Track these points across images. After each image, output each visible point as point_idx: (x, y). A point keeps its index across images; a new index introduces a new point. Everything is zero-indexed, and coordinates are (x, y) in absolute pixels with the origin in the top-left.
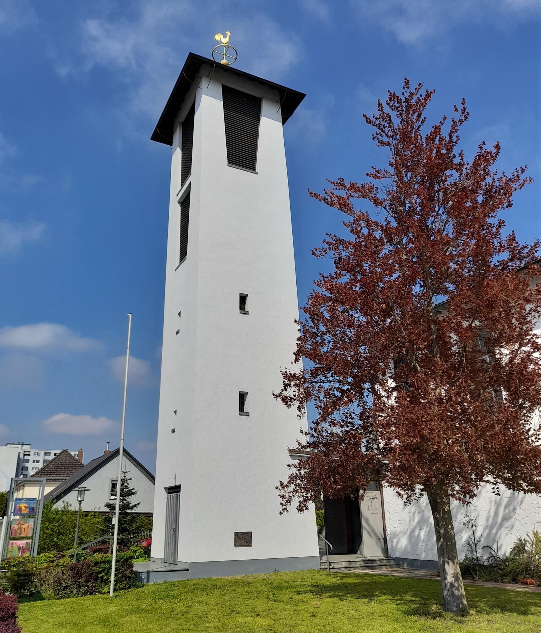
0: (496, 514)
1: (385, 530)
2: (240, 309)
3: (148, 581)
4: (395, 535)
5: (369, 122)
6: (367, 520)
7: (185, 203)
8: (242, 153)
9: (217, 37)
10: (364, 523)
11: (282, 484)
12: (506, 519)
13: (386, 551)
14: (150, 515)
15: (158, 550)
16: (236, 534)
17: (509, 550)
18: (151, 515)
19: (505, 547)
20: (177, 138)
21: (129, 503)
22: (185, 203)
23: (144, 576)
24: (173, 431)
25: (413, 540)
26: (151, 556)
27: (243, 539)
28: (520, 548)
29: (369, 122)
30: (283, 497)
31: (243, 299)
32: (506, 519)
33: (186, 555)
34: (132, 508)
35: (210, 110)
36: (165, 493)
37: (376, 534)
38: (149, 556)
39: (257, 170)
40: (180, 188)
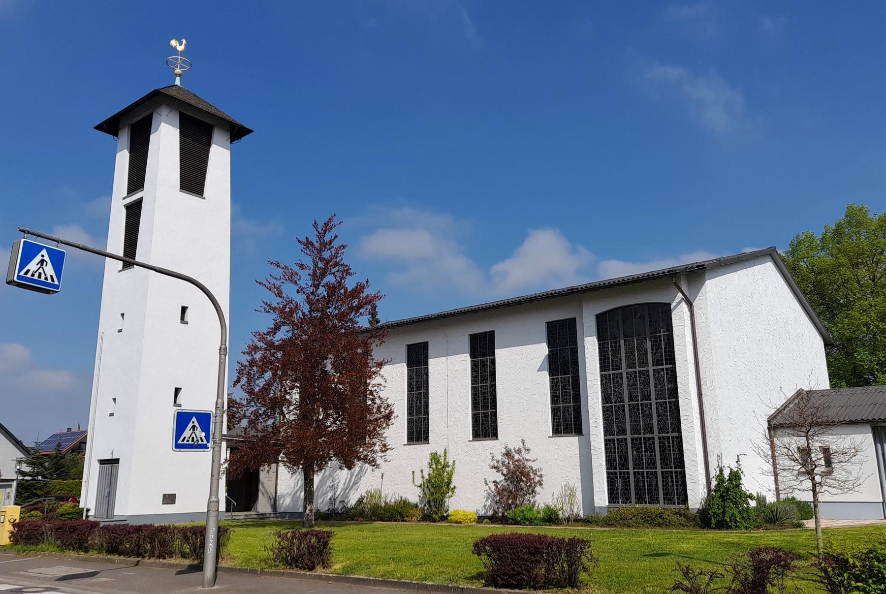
0: (350, 480)
1: (276, 492)
4: (283, 496)
5: (299, 242)
6: (263, 484)
7: (134, 211)
8: (193, 180)
9: (174, 43)
10: (260, 487)
12: (355, 483)
13: (274, 507)
16: (164, 495)
17: (354, 503)
19: (352, 501)
22: (134, 211)
25: (294, 498)
27: (169, 499)
28: (360, 501)
29: (299, 242)
31: (184, 309)
32: (355, 483)
35: (166, 140)
36: (98, 465)
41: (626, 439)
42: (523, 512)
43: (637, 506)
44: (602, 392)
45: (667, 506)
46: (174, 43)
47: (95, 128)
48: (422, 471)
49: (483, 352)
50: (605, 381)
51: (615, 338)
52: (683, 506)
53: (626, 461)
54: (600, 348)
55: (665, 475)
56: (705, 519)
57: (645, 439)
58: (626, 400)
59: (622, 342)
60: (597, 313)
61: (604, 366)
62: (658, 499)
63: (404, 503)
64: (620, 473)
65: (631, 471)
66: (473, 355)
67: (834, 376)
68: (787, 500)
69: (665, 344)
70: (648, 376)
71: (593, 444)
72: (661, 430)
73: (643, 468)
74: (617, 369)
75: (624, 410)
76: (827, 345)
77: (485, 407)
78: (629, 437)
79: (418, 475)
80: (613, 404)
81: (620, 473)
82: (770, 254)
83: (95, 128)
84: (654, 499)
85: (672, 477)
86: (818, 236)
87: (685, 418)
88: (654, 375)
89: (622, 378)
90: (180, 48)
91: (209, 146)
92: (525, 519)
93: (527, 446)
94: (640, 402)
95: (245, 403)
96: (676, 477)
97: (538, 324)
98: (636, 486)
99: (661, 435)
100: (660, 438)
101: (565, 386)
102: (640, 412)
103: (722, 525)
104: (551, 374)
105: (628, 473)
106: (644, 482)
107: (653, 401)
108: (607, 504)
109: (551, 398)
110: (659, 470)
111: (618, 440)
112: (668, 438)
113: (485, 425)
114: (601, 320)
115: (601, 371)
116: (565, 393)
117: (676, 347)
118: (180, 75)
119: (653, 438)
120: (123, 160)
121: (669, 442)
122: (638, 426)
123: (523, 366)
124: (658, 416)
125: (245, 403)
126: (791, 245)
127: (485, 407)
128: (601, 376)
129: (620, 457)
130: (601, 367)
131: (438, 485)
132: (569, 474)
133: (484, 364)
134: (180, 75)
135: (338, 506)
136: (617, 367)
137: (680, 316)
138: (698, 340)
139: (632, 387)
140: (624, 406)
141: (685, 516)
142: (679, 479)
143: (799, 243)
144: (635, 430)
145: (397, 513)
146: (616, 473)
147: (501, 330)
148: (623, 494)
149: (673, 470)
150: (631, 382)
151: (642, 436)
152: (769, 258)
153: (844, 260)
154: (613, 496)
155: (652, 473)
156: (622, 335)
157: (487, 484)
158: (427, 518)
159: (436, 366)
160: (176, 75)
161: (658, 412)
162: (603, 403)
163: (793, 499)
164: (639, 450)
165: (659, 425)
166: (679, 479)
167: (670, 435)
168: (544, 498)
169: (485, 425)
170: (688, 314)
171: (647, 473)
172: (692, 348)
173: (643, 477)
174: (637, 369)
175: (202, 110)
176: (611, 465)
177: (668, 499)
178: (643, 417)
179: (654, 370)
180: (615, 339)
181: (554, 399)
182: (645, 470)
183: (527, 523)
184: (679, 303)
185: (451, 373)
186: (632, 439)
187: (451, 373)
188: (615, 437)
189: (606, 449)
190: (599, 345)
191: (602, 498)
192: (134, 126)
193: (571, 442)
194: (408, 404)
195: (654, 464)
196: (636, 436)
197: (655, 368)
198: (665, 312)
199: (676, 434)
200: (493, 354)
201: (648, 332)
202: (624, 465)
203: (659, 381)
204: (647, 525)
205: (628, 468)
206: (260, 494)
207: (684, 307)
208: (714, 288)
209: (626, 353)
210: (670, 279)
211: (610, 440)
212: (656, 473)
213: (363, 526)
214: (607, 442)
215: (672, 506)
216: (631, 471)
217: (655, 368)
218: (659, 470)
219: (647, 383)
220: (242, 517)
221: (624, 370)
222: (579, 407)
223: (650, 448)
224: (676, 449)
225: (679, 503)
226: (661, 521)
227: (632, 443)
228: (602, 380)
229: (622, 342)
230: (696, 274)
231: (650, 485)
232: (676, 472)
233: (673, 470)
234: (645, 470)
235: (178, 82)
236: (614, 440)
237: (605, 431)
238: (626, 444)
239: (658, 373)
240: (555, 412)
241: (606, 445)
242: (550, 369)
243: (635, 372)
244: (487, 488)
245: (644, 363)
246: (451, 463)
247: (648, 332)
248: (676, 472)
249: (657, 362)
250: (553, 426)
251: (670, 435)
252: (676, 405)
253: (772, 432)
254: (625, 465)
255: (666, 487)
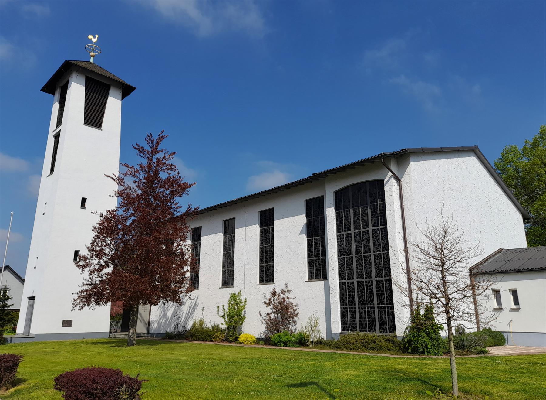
2: (82, 206)
3: (11, 342)
4: (153, 322)
6: (141, 315)
7: (57, 137)
8: (94, 117)
9: (90, 37)
11: (74, 299)
13: (148, 329)
14: (18, 311)
15: (20, 328)
16: (64, 321)
18: (18, 311)
20: (58, 94)
21: (7, 304)
22: (57, 137)
23: (9, 340)
24: (35, 268)
26: (17, 332)
27: (67, 323)
28: (193, 326)
30: (74, 304)
31: (84, 200)
33: (34, 331)
34: (9, 306)
35: (77, 91)
36: (27, 300)
37: (144, 320)
38: (15, 332)
39: (102, 128)
40: (55, 128)
41: (353, 282)
42: (279, 336)
43: (360, 333)
44: (338, 247)
45: (381, 334)
46: (90, 37)
47: (43, 90)
48: (223, 306)
49: (267, 222)
50: (340, 238)
51: (347, 208)
52: (392, 334)
53: (354, 299)
54: (337, 216)
55: (380, 310)
56: (408, 346)
57: (366, 282)
58: (354, 253)
59: (351, 210)
60: (335, 190)
61: (339, 228)
62: (375, 328)
63: (216, 329)
64: (349, 308)
65: (357, 306)
66: (261, 225)
67: (529, 241)
68: (485, 330)
69: (380, 211)
70: (369, 234)
71: (331, 286)
72: (377, 275)
73: (347, 305)
74: (348, 231)
75: (352, 261)
76: (526, 219)
77: (267, 261)
78: (355, 280)
79: (221, 308)
80: (345, 257)
81: (349, 308)
82: (473, 151)
83: (43, 90)
84: (372, 329)
85: (385, 311)
86: (520, 148)
87: (394, 265)
88: (373, 234)
89: (351, 237)
90: (94, 40)
91: (107, 98)
92: (281, 342)
93: (289, 288)
94: (363, 255)
95: (89, 257)
96: (388, 311)
97: (299, 202)
98: (360, 318)
99: (377, 279)
100: (376, 281)
101: (316, 244)
102: (364, 262)
103: (415, 351)
104: (308, 236)
105: (355, 308)
106: (365, 314)
107: (372, 253)
108: (340, 331)
109: (308, 253)
110: (376, 306)
111: (348, 283)
112: (382, 281)
113: (267, 275)
114: (339, 196)
115: (337, 232)
116: (316, 250)
117: (387, 212)
118: (93, 56)
119: (372, 281)
120: (56, 107)
121: (383, 284)
122: (362, 272)
123: (290, 230)
124: (376, 265)
125: (89, 257)
126: (502, 154)
127: (267, 261)
128: (338, 236)
129: (350, 295)
130: (337, 230)
131: (236, 315)
132: (318, 307)
133: (267, 232)
134: (93, 56)
135: (181, 329)
136: (348, 229)
137: (391, 189)
138: (405, 207)
139: (358, 243)
140: (352, 257)
141: (393, 342)
142: (390, 313)
143: (507, 152)
144: (360, 276)
145: (201, 334)
146: (347, 308)
147: (278, 207)
148: (351, 324)
149: (386, 306)
150: (357, 240)
151: (364, 280)
152: (474, 154)
153: (538, 161)
154: (344, 327)
155: (371, 308)
156: (351, 206)
157: (261, 315)
158: (227, 340)
159: (239, 233)
160: (91, 56)
161: (375, 261)
162: (338, 256)
163: (490, 329)
164: (362, 292)
165: (376, 271)
166: (390, 313)
167: (384, 279)
168: (300, 325)
169: (267, 275)
170: (398, 187)
171: (368, 308)
172: (400, 213)
173: (365, 311)
174: (362, 230)
175: (100, 74)
176: (343, 302)
177: (383, 330)
178: (365, 265)
179: (373, 230)
180: (347, 207)
181: (310, 254)
182: (366, 306)
183: (283, 345)
184: (390, 179)
185: (248, 236)
186: (358, 282)
187: (248, 236)
188: (346, 281)
189: (340, 289)
190: (337, 213)
191: (337, 328)
192: (57, 86)
193: (320, 284)
194: (223, 260)
195: (373, 301)
196: (360, 280)
197: (373, 228)
198: (380, 185)
199: (388, 278)
200: (272, 224)
201: (369, 202)
202: (352, 302)
203: (376, 238)
204: (364, 348)
205: (355, 305)
206: (138, 321)
207: (394, 182)
208: (416, 168)
209: (354, 218)
210: (381, 161)
211: (343, 283)
212: (374, 308)
213: (173, 345)
214: (341, 284)
215: (385, 334)
216: (357, 306)
217: (373, 228)
218: (376, 306)
219: (368, 240)
220: (123, 336)
221: (353, 231)
222: (325, 260)
223: (370, 289)
224: (388, 290)
225: (390, 332)
226: (374, 345)
227: (358, 285)
228: (338, 239)
229: (351, 210)
230: (402, 157)
231: (370, 317)
232: (388, 307)
233: (386, 306)
234: (366, 306)
235: (92, 60)
236: (345, 283)
237: (340, 277)
238: (354, 286)
239: (376, 232)
240: (310, 263)
241: (340, 287)
242: (307, 233)
243: (360, 232)
244: (261, 318)
245: (366, 225)
246: (243, 301)
247: (369, 202)
248: (388, 307)
249: (375, 224)
250: (309, 273)
251: (384, 279)
252: (388, 255)
253: (473, 278)
254: (352, 302)
255: (381, 319)
